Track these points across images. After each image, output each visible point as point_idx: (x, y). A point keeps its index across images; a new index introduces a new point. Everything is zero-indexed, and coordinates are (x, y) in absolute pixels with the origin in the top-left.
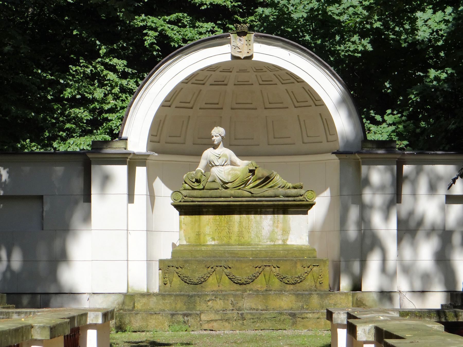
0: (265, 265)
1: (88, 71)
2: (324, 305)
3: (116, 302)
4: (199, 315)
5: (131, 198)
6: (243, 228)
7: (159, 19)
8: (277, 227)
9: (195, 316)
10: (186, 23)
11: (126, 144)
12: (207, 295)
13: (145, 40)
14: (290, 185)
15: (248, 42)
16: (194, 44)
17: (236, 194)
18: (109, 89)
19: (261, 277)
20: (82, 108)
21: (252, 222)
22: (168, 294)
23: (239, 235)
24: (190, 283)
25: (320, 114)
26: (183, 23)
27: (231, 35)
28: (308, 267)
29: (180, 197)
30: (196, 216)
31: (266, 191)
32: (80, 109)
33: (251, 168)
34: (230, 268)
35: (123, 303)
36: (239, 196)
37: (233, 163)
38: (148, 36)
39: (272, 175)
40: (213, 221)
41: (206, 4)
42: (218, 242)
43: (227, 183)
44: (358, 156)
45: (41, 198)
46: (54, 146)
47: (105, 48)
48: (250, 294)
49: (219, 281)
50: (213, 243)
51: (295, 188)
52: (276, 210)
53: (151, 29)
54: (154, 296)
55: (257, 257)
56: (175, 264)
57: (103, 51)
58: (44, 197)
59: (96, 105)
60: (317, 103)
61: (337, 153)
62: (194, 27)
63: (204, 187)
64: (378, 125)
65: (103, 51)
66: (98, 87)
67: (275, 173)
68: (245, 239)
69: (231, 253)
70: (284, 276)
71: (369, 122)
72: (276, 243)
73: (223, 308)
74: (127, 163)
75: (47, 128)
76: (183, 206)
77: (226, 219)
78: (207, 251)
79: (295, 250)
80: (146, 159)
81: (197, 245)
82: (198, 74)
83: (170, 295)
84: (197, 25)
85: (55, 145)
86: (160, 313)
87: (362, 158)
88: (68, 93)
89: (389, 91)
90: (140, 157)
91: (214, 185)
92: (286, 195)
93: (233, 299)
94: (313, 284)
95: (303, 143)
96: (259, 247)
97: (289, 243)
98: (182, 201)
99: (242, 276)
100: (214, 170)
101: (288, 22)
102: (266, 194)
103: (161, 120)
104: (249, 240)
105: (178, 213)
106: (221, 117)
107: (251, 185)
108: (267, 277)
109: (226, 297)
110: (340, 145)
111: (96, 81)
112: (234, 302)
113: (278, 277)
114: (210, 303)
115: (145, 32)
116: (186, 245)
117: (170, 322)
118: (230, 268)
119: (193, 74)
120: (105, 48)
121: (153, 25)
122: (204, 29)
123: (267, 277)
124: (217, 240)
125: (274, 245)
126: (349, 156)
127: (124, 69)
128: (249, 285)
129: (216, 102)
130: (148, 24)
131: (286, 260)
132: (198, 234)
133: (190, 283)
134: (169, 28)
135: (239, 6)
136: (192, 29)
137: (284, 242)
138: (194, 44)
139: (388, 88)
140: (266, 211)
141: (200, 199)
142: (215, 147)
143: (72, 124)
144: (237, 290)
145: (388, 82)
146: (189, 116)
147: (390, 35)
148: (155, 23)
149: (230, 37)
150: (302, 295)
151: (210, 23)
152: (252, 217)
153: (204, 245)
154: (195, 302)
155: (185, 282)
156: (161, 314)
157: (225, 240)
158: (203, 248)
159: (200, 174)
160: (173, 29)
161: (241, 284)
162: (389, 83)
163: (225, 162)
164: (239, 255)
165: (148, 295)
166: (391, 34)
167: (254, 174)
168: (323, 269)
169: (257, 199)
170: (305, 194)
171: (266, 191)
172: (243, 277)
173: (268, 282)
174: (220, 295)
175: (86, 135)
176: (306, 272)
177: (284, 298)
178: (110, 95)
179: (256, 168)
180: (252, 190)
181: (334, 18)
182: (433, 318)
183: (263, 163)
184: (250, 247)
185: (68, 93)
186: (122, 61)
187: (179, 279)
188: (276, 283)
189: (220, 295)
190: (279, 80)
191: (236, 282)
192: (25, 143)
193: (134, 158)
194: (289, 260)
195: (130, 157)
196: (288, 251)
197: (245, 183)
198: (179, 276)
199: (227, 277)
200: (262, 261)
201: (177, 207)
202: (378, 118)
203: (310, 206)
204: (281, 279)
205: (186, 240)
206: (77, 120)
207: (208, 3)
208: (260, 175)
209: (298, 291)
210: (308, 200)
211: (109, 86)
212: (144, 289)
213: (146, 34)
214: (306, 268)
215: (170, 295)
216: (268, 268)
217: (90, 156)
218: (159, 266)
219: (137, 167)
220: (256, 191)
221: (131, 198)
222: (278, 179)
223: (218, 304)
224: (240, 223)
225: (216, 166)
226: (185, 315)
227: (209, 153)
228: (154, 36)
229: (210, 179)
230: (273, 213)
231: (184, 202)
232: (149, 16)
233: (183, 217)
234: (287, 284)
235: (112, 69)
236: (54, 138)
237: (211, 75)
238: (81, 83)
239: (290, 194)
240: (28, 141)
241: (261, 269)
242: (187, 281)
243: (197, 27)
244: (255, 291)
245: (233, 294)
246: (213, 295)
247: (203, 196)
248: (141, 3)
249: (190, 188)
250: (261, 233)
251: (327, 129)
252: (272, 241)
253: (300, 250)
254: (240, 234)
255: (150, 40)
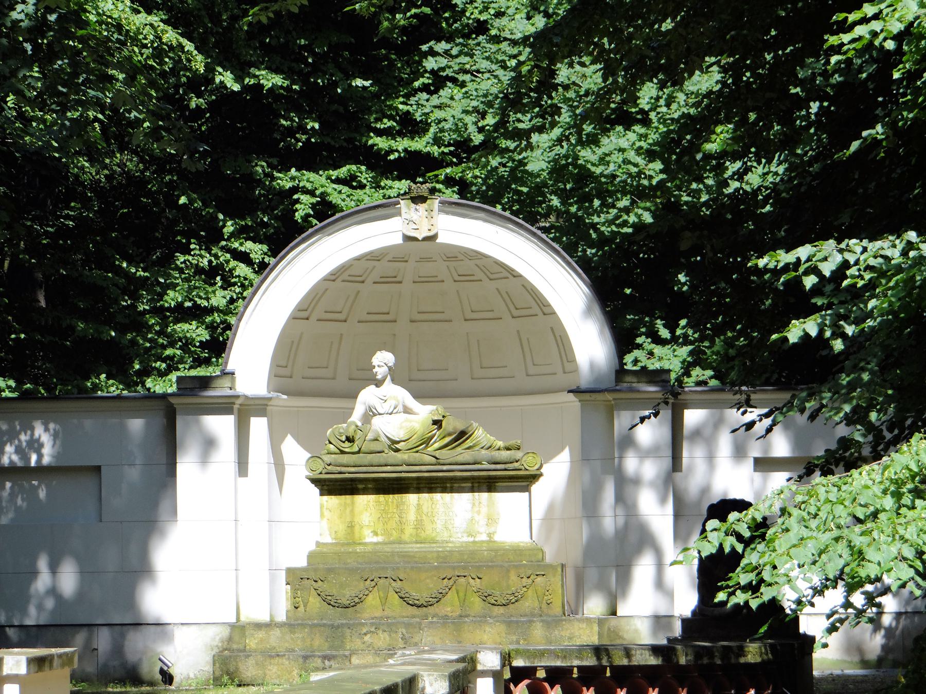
0: (459, 574)
1: (205, 263)
2: (553, 638)
3: (218, 638)
4: (348, 658)
5: (242, 466)
6: (424, 516)
7: (321, 176)
8: (479, 512)
9: (343, 659)
10: (365, 181)
11: (233, 381)
12: (363, 624)
13: (297, 210)
14: (500, 444)
15: (429, 214)
16: (342, 218)
17: (412, 461)
18: (238, 290)
19: (452, 595)
20: (194, 323)
21: (438, 506)
22: (299, 624)
23: (418, 526)
24: (337, 605)
25: (552, 329)
26: (360, 181)
27: (401, 201)
28: (528, 578)
29: (319, 466)
30: (347, 496)
31: (461, 454)
32: (191, 324)
33: (436, 418)
34: (401, 580)
35: (230, 639)
36: (418, 463)
37: (407, 410)
38: (301, 203)
39: (470, 429)
40: (375, 504)
41: (397, 151)
42: (383, 537)
43: (398, 442)
44: (609, 397)
45: (97, 469)
46: (147, 386)
47: (232, 225)
48: (432, 622)
49: (384, 601)
50: (375, 539)
51: (508, 449)
52: (476, 485)
53: (306, 191)
54: (277, 627)
55: (446, 563)
56: (312, 575)
57: (229, 228)
58: (103, 469)
59: (217, 317)
60: (546, 310)
61: (576, 391)
62: (378, 187)
63: (360, 449)
64: (664, 346)
65: (229, 228)
66: (221, 287)
67: (475, 425)
68: (428, 532)
69: (404, 556)
70: (489, 592)
71: (649, 340)
72: (477, 539)
73: (389, 645)
74: (235, 411)
75: (137, 356)
76: (325, 480)
77: (395, 501)
78: (365, 553)
79: (507, 550)
80: (267, 405)
81: (348, 544)
82: (352, 265)
83: (303, 626)
84: (382, 184)
85: (149, 383)
86: (284, 655)
87: (614, 399)
88: (172, 298)
89: (685, 288)
90: (257, 402)
91: (376, 446)
92: (493, 461)
93: (404, 631)
94: (536, 604)
95: (528, 375)
96: (450, 545)
97: (497, 538)
98: (323, 472)
99: (420, 594)
100: (376, 422)
101: (522, 177)
102: (460, 459)
103: (293, 342)
104: (434, 535)
105: (317, 491)
106: (394, 335)
107: (437, 445)
108: (461, 594)
109: (394, 628)
110: (585, 378)
111: (218, 278)
112: (407, 635)
113: (480, 593)
114: (367, 638)
115: (295, 197)
116: (332, 544)
117: (301, 669)
118: (401, 580)
119: (343, 267)
120: (232, 225)
121: (309, 186)
122: (394, 190)
123: (461, 594)
124: (382, 535)
125: (474, 542)
126: (594, 396)
127: (263, 259)
128: (432, 607)
129: (386, 311)
130: (301, 184)
131: (492, 567)
132: (351, 526)
133: (337, 605)
134: (336, 190)
135: (451, 153)
136: (374, 190)
137: (490, 537)
138: (342, 218)
139: (685, 284)
140: (459, 487)
141: (353, 469)
142: (379, 383)
143: (177, 349)
144: (414, 617)
145: (683, 274)
146: (341, 334)
147: (682, 196)
148: (312, 182)
149: (399, 206)
150: (517, 622)
151: (404, 181)
152: (437, 496)
153: (360, 544)
154: (342, 636)
155: (329, 604)
156: (287, 657)
157: (395, 535)
158: (359, 549)
159: (353, 427)
160: (340, 192)
161: (419, 607)
162: (686, 276)
163: (395, 408)
164: (416, 559)
165: (269, 625)
166: (685, 194)
167: (440, 427)
168: (552, 579)
169: (445, 468)
170: (524, 459)
171: (461, 454)
172: (422, 595)
173: (463, 602)
174: (383, 624)
175: (200, 366)
176: (524, 585)
177: (488, 629)
178: (240, 300)
179: (444, 417)
180: (437, 454)
181: (589, 169)
182: (587, 660)
183: (465, 408)
184: (434, 545)
185: (172, 298)
186: (260, 246)
187: (319, 599)
188: (477, 604)
189: (383, 624)
190: (484, 273)
191: (410, 602)
192: (97, 381)
193: (246, 403)
194: (497, 566)
195: (239, 402)
196: (496, 551)
197: (427, 441)
198: (319, 595)
199: (396, 595)
200: (454, 568)
201: (315, 481)
202: (665, 333)
203: (534, 477)
204: (485, 598)
205: (330, 535)
206: (187, 344)
207: (400, 149)
208: (450, 429)
209: (511, 616)
210: (528, 468)
211: (239, 287)
212: (265, 618)
213: (297, 201)
214: (525, 580)
215: (302, 624)
216: (462, 580)
217: (173, 400)
218: (286, 579)
219: (252, 418)
220: (445, 454)
221: (242, 466)
222: (480, 435)
223: (380, 639)
224: (419, 507)
225: (380, 414)
226: (325, 657)
227: (368, 396)
228: (311, 204)
229: (370, 436)
230: (472, 490)
231: (327, 473)
232: (305, 172)
233: (325, 498)
234: (493, 604)
235: (244, 258)
236: (146, 372)
237: (374, 267)
238: (193, 282)
239: (498, 460)
240: (103, 376)
241: (451, 582)
242: (332, 603)
243: (383, 188)
244: (442, 617)
245: (404, 623)
246: (372, 624)
247: (358, 463)
248: (201, 149)
249: (338, 451)
250: (452, 522)
251: (563, 353)
252: (470, 535)
253: (518, 551)
254: (419, 525)
255: (304, 210)
